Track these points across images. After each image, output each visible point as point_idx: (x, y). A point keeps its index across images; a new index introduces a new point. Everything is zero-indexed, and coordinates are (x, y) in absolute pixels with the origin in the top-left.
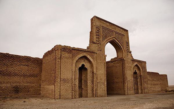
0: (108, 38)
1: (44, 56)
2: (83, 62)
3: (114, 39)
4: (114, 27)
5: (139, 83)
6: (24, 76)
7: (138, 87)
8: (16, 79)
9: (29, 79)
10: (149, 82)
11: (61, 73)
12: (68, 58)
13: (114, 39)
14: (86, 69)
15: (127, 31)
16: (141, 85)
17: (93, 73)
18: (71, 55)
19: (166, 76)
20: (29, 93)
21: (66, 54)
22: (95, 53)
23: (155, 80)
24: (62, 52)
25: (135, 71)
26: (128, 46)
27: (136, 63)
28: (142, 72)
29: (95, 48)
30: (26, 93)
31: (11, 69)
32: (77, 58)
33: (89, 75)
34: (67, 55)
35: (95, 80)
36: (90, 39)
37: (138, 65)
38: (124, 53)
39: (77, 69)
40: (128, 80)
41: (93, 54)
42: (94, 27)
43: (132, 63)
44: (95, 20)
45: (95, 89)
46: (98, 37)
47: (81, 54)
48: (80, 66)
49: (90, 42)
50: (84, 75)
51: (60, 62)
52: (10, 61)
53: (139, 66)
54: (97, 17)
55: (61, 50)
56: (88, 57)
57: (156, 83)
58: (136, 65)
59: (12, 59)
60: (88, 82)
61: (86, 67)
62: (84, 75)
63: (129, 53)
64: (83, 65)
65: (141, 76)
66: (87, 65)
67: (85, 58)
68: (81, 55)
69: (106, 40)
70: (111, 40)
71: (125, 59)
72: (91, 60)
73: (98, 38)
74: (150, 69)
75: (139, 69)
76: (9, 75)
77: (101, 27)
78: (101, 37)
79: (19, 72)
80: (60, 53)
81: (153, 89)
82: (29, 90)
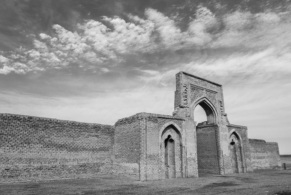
1: (117, 124)
2: (170, 132)
3: (205, 99)
5: (238, 158)
6: (94, 150)
7: (237, 163)
9: (98, 155)
10: (252, 154)
13: (205, 99)
14: (172, 141)
15: (220, 86)
16: (242, 161)
17: (181, 145)
18: (157, 124)
19: (276, 144)
20: (98, 173)
22: (183, 120)
25: (233, 140)
26: (222, 107)
27: (233, 130)
28: (241, 142)
29: (181, 113)
31: (78, 142)
32: (163, 128)
35: (184, 155)
36: (175, 101)
37: (236, 132)
38: (217, 117)
39: (163, 141)
40: (223, 154)
41: (181, 121)
43: (227, 130)
45: (184, 167)
46: (186, 98)
48: (166, 137)
49: (175, 105)
52: (77, 132)
53: (238, 134)
55: (146, 119)
56: (176, 125)
57: (260, 155)
58: (234, 133)
59: (79, 129)
63: (223, 117)
64: (169, 136)
65: (240, 148)
66: (174, 136)
67: (172, 126)
69: (195, 102)
70: (201, 100)
71: (218, 125)
72: (179, 129)
73: (186, 100)
74: (251, 135)
75: (237, 138)
76: (76, 149)
77: (190, 87)
78: (190, 99)
79: (87, 145)
80: (145, 124)
81: (258, 165)
82: (99, 168)
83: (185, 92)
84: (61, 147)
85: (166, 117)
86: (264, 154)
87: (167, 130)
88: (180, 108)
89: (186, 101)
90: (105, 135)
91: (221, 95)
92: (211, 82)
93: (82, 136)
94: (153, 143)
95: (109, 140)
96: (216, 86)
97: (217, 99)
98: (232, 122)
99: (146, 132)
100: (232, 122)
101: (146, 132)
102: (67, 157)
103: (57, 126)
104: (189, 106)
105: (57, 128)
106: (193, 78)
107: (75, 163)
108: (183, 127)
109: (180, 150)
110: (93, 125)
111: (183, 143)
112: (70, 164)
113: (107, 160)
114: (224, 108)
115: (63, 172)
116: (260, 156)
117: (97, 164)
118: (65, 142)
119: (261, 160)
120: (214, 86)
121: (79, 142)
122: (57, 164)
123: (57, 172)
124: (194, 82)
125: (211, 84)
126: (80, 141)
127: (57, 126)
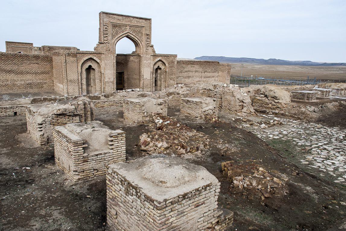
0: (120, 35)
2: (89, 63)
3: (128, 34)
4: (129, 19)
8: (29, 77)
9: (41, 77)
11: (68, 75)
12: (73, 62)
15: (150, 20)
20: (43, 89)
21: (71, 59)
23: (210, 71)
24: (66, 58)
30: (41, 89)
31: (22, 68)
33: (97, 75)
34: (72, 59)
42: (102, 25)
44: (104, 14)
45: (102, 88)
47: (86, 56)
50: (93, 75)
51: (65, 66)
53: (164, 61)
54: (104, 13)
56: (95, 58)
60: (96, 81)
61: (93, 67)
62: (93, 75)
63: (149, 48)
64: (90, 66)
66: (94, 66)
68: (87, 58)
71: (141, 55)
72: (98, 61)
76: (21, 73)
79: (30, 70)
80: (65, 59)
83: (106, 30)
84: (10, 72)
85: (84, 52)
86: (214, 73)
87: (88, 62)
88: (99, 44)
89: (107, 38)
90: (45, 62)
91: (150, 28)
92: (137, 18)
93: (24, 64)
94: (75, 72)
95: (49, 66)
96: (144, 21)
97: (143, 33)
98: (158, 51)
99: (66, 64)
100: (157, 52)
101: (66, 64)
102: (15, 79)
103: (3, 57)
104: (110, 42)
105: (3, 59)
106: (115, 16)
107: (23, 83)
108: (103, 59)
109: (100, 76)
110: (33, 55)
111: (102, 71)
112: (18, 83)
113: (48, 80)
114: (151, 40)
115: (15, 88)
116: (208, 75)
117: (41, 83)
118: (12, 68)
119: (209, 79)
120: (141, 21)
121: (23, 68)
122: (9, 83)
123: (10, 88)
124: (116, 20)
125: (136, 19)
126: (24, 67)
127: (3, 57)
